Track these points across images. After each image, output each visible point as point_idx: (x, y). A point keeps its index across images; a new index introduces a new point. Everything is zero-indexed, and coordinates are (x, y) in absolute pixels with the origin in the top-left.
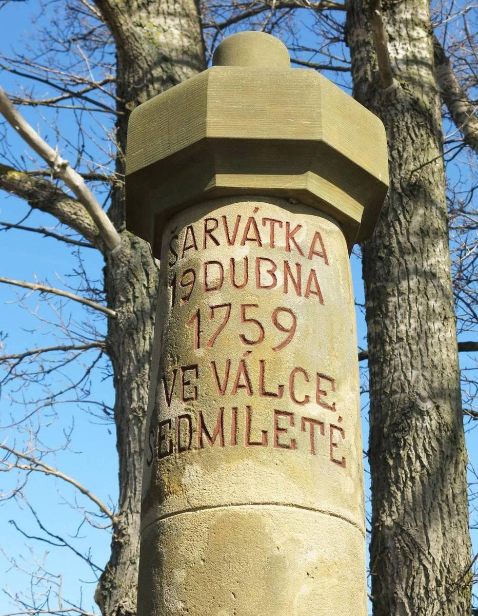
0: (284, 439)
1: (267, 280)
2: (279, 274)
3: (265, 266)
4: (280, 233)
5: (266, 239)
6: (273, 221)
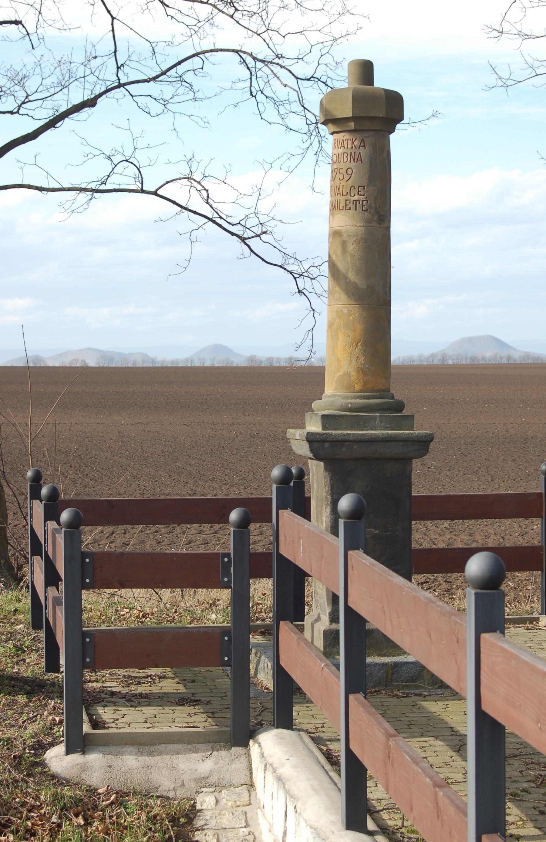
0: (348, 207)
1: (345, 160)
2: (349, 157)
3: (346, 155)
4: (350, 142)
5: (346, 146)
6: (348, 139)
